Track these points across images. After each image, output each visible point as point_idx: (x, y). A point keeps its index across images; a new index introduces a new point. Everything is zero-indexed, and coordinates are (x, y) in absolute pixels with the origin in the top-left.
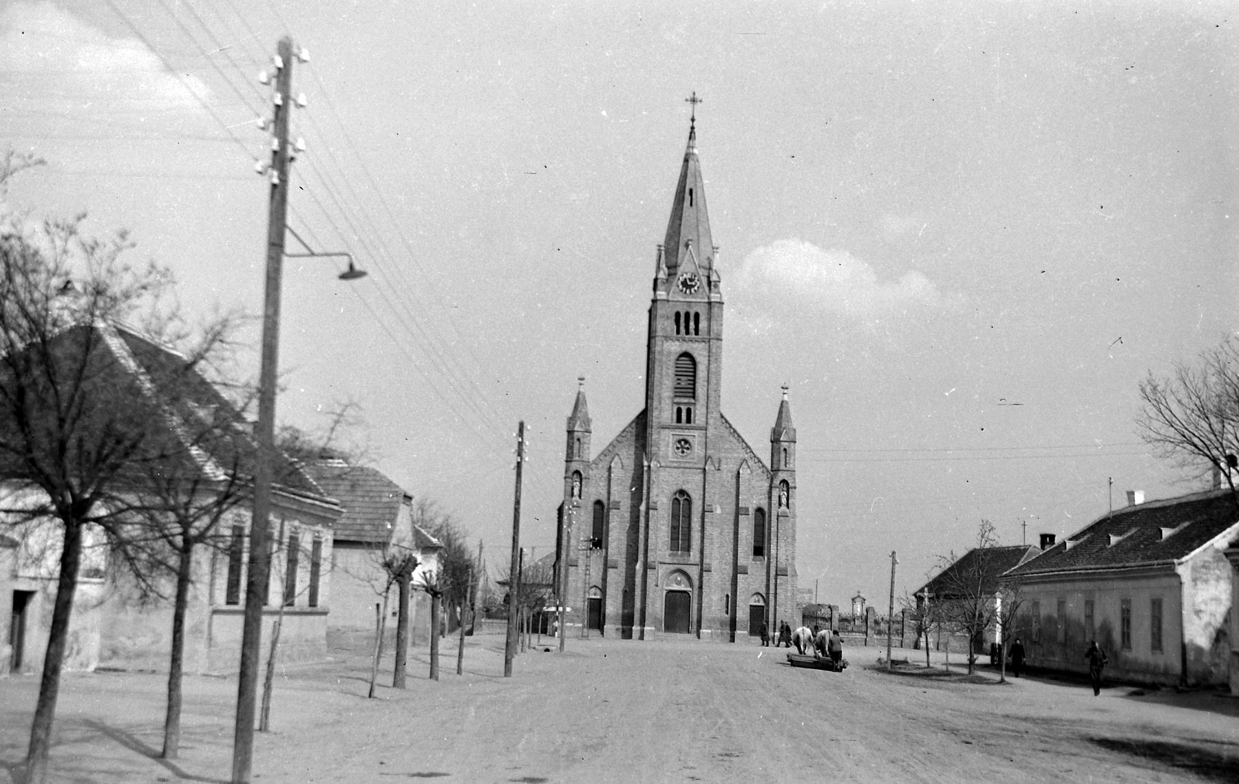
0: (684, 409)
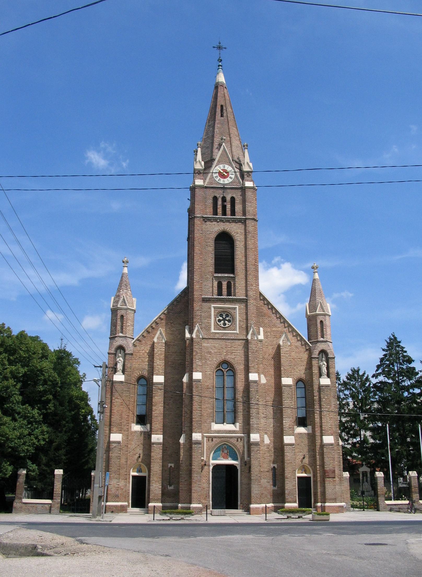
0: (225, 284)
